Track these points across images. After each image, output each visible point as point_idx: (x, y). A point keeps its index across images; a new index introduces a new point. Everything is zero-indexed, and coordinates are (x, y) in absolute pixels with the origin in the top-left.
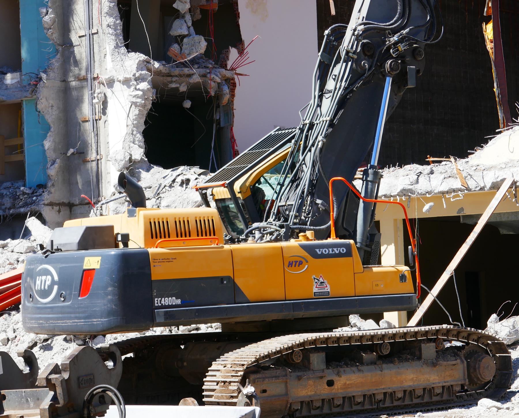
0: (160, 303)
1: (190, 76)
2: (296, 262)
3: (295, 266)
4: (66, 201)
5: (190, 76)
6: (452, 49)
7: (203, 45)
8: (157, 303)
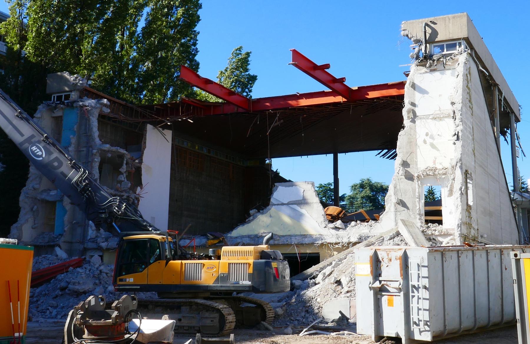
7: (130, 184)
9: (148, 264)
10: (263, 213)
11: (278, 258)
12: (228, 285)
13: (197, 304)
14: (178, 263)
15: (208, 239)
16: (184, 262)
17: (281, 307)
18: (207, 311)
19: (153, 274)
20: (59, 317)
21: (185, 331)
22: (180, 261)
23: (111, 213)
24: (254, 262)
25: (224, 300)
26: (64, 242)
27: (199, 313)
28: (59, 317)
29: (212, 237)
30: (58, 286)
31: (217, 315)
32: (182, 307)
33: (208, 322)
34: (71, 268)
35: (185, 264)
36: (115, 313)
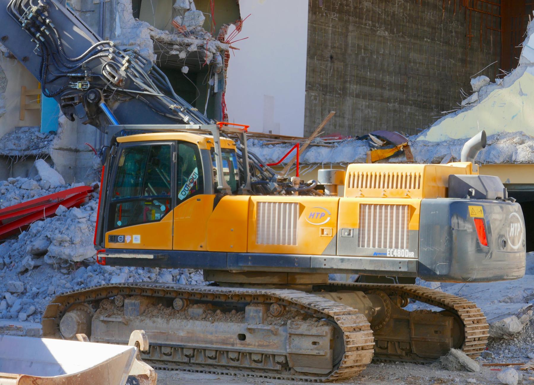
0: (392, 254)
1: (188, 45)
2: (318, 214)
3: (317, 218)
4: (73, 147)
5: (188, 45)
6: (429, 40)
8: (389, 254)
10: (502, 86)
13: (280, 300)
14: (242, 202)
15: (371, 147)
16: (256, 198)
17: (518, 316)
18: (305, 319)
19: (185, 225)
21: (254, 365)
23: (97, 79)
25: (361, 294)
26: (60, 149)
27: (285, 324)
28: (23, 315)
29: (380, 143)
30: (29, 248)
31: (326, 330)
32: (247, 308)
33: (305, 346)
34: (62, 208)
35: (258, 203)
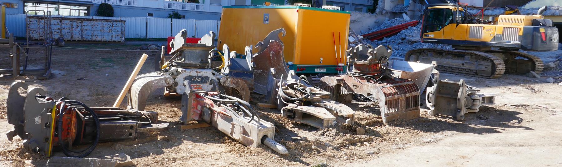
9: (443, 26)
11: (547, 25)
12: (503, 43)
16: (469, 25)
17: (554, 62)
19: (449, 32)
20: (398, 55)
22: (466, 25)
24: (525, 29)
31: (490, 64)
33: (483, 68)
34: (410, 27)
36: (371, 57)
